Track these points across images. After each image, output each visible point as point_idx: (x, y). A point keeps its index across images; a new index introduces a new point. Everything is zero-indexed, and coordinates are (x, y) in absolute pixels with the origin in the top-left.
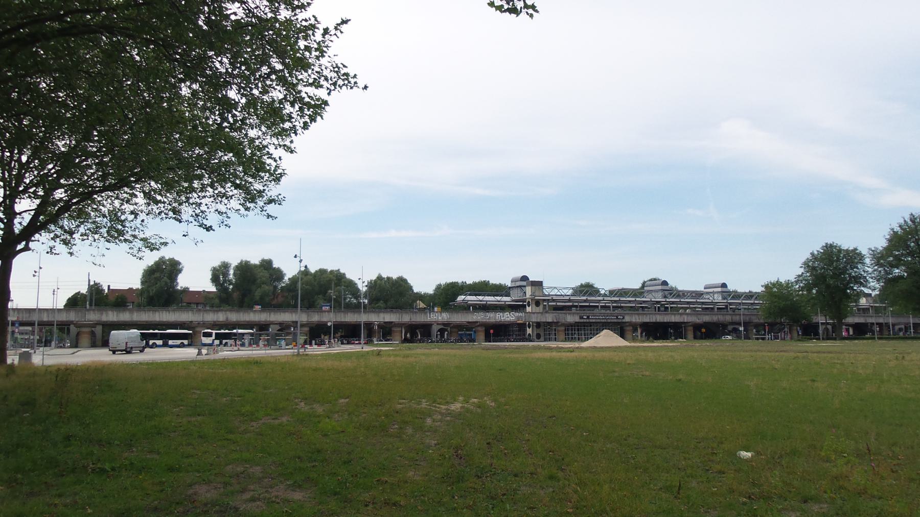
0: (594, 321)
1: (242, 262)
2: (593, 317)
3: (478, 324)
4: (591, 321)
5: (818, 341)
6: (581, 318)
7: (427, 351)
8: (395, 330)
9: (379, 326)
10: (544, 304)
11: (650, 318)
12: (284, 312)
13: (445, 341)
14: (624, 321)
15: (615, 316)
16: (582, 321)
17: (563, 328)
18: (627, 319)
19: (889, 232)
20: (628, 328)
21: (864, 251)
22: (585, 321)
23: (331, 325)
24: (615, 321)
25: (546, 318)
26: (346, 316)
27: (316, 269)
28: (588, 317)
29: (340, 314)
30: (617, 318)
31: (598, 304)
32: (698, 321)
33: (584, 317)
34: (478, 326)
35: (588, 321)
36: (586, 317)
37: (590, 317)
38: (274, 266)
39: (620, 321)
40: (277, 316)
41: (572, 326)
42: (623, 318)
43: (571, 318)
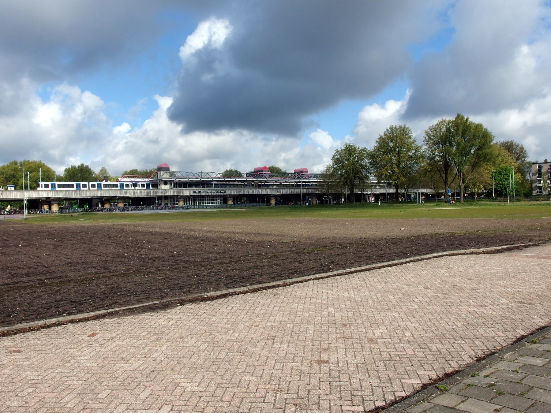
0: (204, 194)
1: (83, 165)
2: (203, 192)
4: (202, 194)
5: (458, 204)
6: (195, 192)
7: (46, 223)
9: (28, 201)
11: (244, 192)
14: (226, 194)
15: (218, 191)
16: (196, 194)
18: (228, 192)
19: (418, 145)
22: (198, 194)
24: (219, 194)
26: (11, 194)
28: (200, 192)
29: (6, 192)
30: (221, 192)
31: (219, 183)
32: (277, 193)
33: (197, 192)
35: (199, 194)
36: (198, 192)
37: (201, 192)
38: (31, 162)
39: (222, 194)
42: (225, 192)
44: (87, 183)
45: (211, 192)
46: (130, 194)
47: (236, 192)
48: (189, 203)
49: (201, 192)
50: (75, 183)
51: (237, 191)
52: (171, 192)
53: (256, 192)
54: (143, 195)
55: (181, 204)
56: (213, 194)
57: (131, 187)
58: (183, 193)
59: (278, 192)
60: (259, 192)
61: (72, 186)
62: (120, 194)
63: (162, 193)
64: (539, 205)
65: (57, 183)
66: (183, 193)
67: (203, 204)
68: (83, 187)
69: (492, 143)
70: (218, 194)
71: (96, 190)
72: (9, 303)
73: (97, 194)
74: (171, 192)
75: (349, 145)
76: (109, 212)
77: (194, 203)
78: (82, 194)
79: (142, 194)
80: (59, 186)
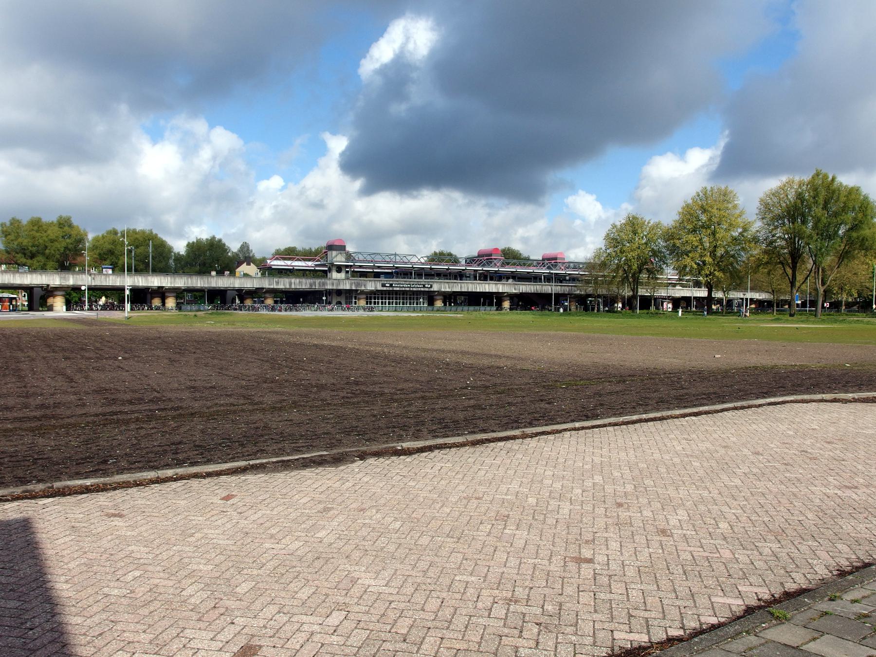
0: (398, 289)
1: (214, 237)
3: (506, 294)
4: (395, 289)
6: (384, 285)
8: (169, 295)
10: (347, 270)
12: (157, 276)
13: (734, 314)
16: (385, 289)
17: (364, 296)
18: (436, 288)
20: (438, 297)
21: (119, 232)
22: (388, 289)
23: (85, 290)
24: (422, 289)
25: (53, 279)
27: (227, 244)
28: (391, 285)
30: (424, 287)
32: (514, 291)
33: (387, 285)
34: (265, 293)
35: (391, 289)
36: (389, 285)
37: (394, 285)
39: (427, 289)
40: (84, 276)
41: (375, 294)
42: (431, 287)
43: (371, 285)
45: (409, 286)
46: (284, 285)
47: (449, 288)
51: (451, 285)
53: (480, 289)
54: (304, 287)
56: (411, 289)
58: (365, 286)
59: (515, 289)
60: (485, 289)
62: (269, 285)
63: (333, 284)
66: (365, 286)
70: (419, 289)
73: (234, 283)
79: (302, 285)
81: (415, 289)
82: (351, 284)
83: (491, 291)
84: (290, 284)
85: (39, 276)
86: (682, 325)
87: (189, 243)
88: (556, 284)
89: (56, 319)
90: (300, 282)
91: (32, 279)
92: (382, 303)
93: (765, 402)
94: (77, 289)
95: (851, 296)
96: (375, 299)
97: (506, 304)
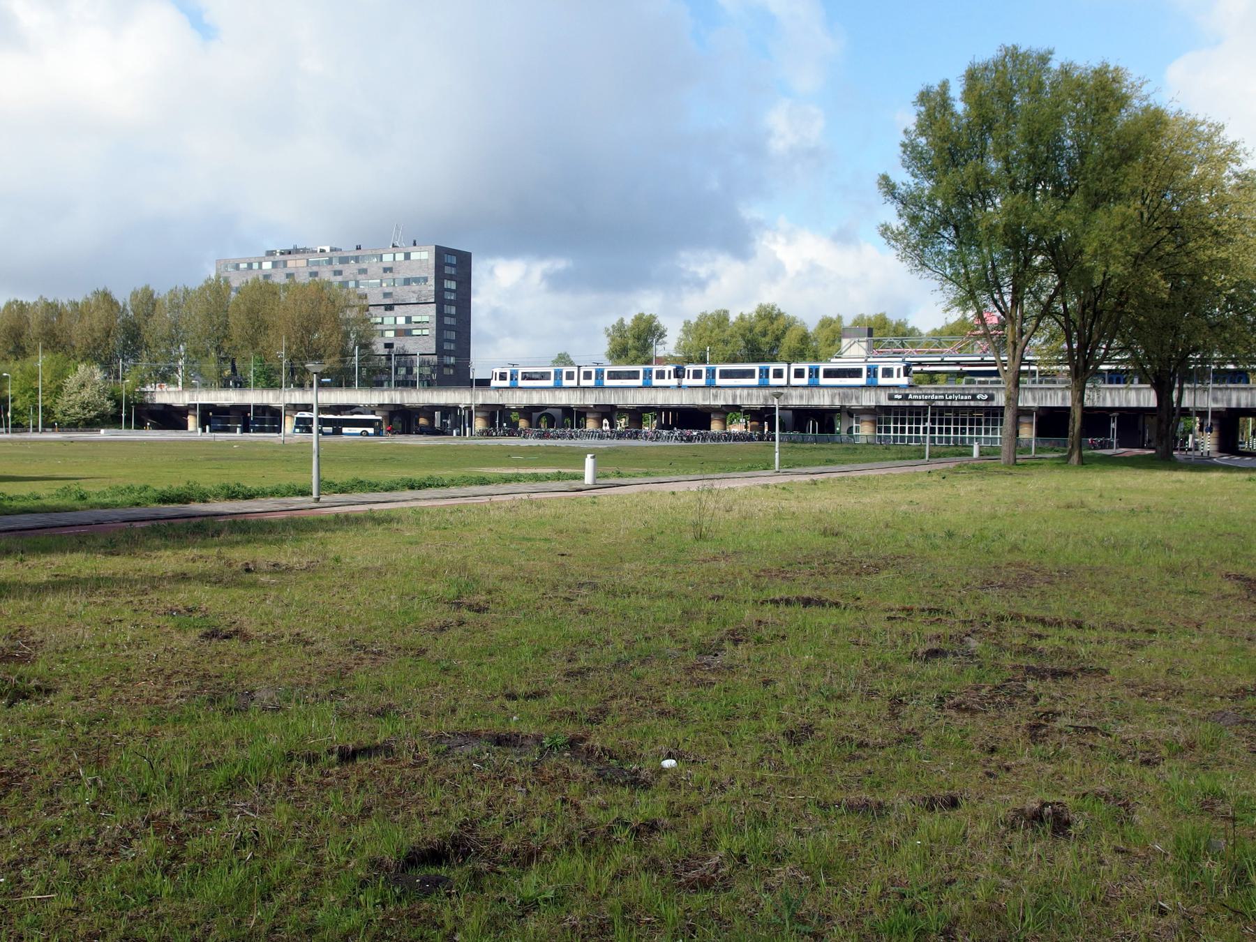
2: (915, 397)
4: (915, 403)
14: (994, 404)
16: (895, 403)
22: (901, 403)
30: (974, 398)
33: (896, 397)
35: (907, 403)
37: (910, 397)
42: (991, 398)
44: (784, 367)
45: (942, 397)
46: (725, 399)
47: (1034, 399)
48: (987, 432)
49: (910, 397)
50: (756, 367)
51: (1038, 394)
52: (826, 396)
53: (1113, 401)
54: (754, 402)
55: (865, 430)
56: (949, 404)
57: (898, 376)
58: (857, 398)
59: (1215, 400)
60: (1129, 402)
61: (750, 374)
62: (704, 400)
63: (801, 397)
64: (356, 460)
65: (719, 368)
66: (857, 398)
67: (895, 431)
68: (883, 376)
69: (959, 107)
70: (966, 404)
71: (862, 387)
72: (1150, 716)
73: (655, 398)
74: (826, 396)
75: (12, 328)
76: (683, 443)
77: (910, 430)
78: (1104, 399)
79: (751, 400)
80: (725, 374)
81: (956, 404)
82: (833, 397)
83: (1142, 405)
84: (734, 398)
85: (364, 396)
86: (951, 466)
87: (687, 323)
88: (1216, 385)
89: (547, 452)
90: (748, 394)
91: (402, 397)
92: (910, 429)
93: (86, 573)
94: (455, 408)
95: (92, 372)
96: (910, 423)
97: (192, 421)
